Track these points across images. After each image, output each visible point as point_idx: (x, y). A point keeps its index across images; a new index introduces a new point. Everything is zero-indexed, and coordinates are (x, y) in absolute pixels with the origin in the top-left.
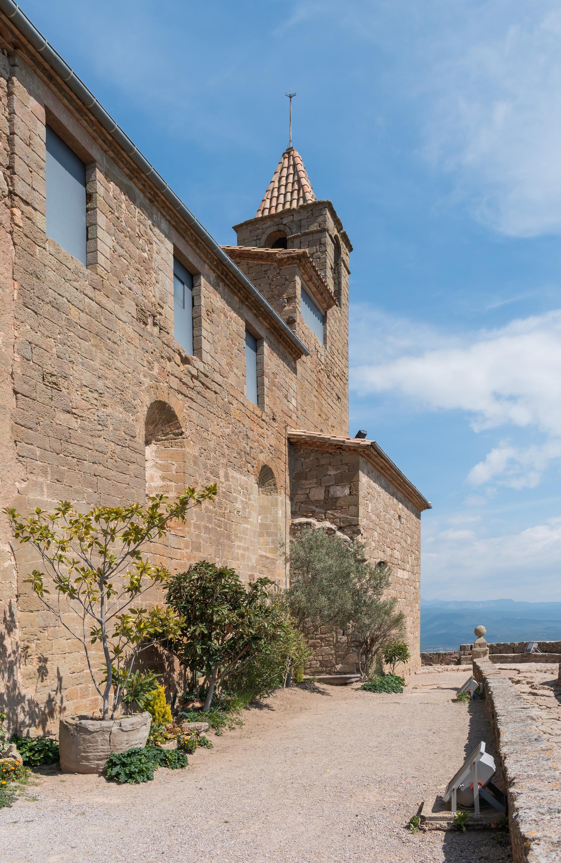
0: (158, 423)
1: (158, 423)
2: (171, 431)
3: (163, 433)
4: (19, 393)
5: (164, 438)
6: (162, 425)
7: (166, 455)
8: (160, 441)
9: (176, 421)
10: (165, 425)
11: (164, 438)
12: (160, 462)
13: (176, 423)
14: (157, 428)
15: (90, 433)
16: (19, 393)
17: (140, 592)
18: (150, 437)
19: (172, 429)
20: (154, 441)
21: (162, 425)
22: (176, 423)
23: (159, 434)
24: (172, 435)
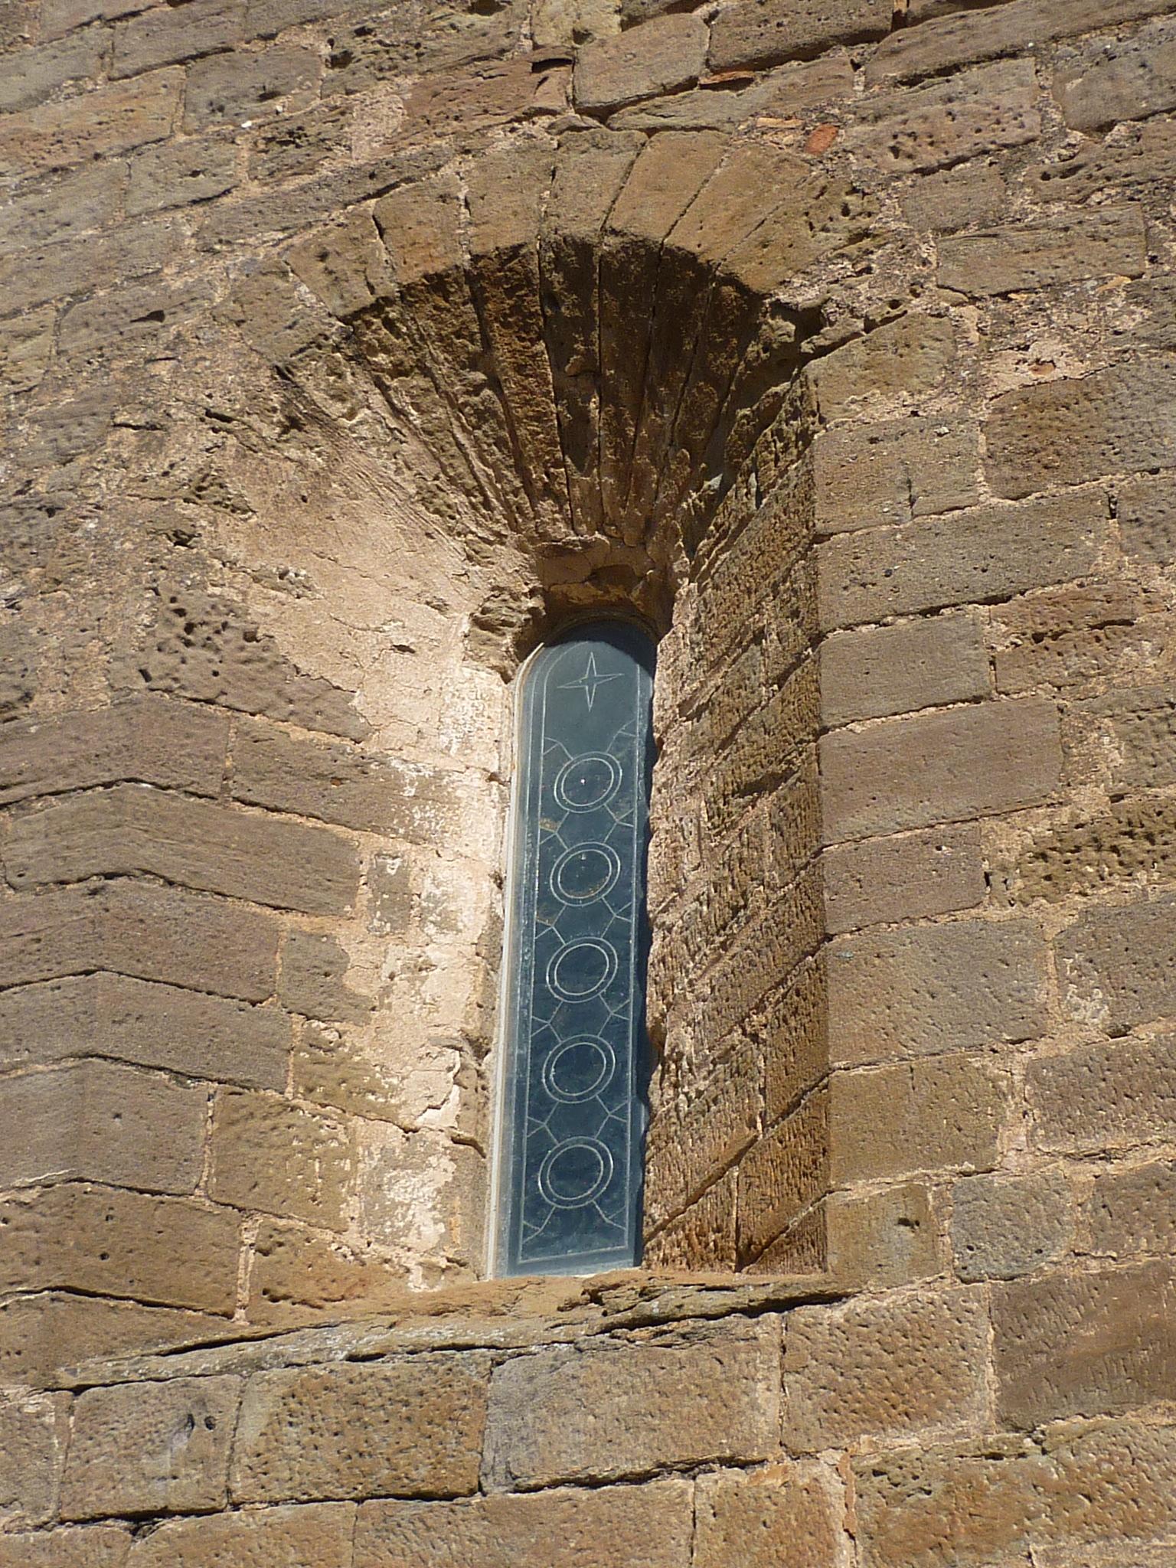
20: (681, 563)
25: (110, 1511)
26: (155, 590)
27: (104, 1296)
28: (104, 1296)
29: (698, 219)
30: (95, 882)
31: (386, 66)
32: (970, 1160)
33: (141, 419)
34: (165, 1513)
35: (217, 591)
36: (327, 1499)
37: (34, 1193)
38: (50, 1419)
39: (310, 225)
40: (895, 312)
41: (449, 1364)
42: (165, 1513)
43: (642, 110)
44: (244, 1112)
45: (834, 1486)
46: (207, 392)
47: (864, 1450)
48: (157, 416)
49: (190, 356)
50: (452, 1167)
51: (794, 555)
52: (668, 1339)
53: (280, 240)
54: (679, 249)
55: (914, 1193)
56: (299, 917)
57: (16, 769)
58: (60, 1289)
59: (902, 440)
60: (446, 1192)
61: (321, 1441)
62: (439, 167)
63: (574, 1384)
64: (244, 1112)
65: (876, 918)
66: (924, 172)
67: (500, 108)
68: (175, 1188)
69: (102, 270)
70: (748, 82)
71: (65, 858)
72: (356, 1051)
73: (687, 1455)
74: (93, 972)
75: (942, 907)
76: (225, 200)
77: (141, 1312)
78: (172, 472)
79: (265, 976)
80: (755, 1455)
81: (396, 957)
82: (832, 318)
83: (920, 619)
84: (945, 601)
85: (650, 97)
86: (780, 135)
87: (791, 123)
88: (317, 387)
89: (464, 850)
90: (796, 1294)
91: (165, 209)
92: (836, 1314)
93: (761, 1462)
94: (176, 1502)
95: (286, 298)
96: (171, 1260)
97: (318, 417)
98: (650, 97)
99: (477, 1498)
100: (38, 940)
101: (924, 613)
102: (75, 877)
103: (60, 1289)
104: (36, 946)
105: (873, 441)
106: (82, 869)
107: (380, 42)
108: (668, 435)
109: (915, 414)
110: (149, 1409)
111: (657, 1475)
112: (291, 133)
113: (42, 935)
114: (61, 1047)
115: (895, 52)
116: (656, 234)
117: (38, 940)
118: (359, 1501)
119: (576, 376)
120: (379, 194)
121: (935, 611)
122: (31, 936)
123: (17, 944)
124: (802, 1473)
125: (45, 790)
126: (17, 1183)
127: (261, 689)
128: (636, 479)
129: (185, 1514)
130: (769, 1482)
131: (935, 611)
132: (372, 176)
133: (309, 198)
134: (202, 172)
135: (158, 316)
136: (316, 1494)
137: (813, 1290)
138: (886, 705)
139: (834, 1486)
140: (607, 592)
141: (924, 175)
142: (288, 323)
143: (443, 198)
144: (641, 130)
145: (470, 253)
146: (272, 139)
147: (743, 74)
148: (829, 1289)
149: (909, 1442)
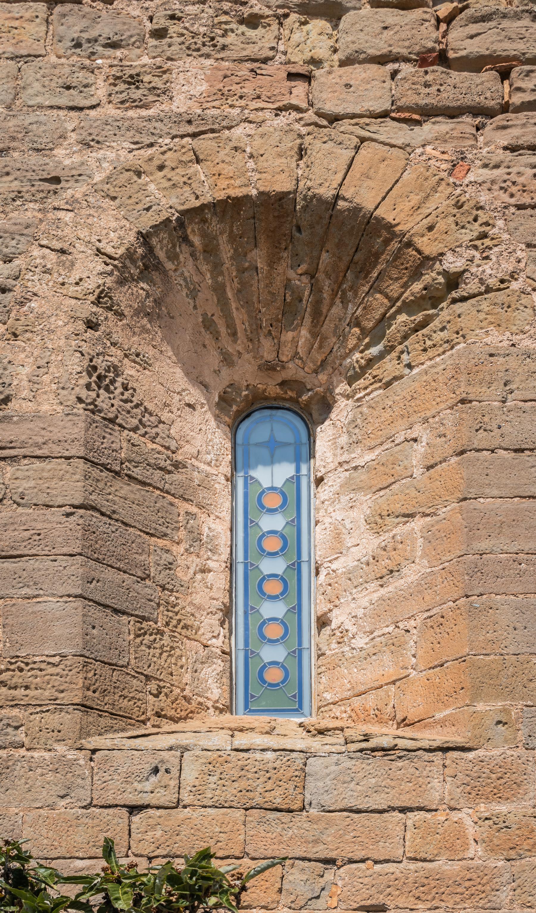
0: (318, 303)
1: (318, 303)
2: (393, 301)
3: (364, 332)
4: (448, 25)
5: (374, 351)
6: (345, 302)
7: (386, 415)
8: (364, 369)
9: (394, 245)
10: (354, 289)
11: (374, 351)
12: (369, 456)
13: (397, 255)
14: (328, 327)
15: (360, 880)
16: (448, 25)
17: (221, 610)
18: (323, 377)
19: (394, 289)
20: (342, 388)
21: (345, 302)
22: (397, 255)
23: (352, 342)
24: (402, 318)
25: (118, 803)
26: (81, 352)
27: (96, 709)
28: (96, 709)
29: (393, 202)
30: (68, 509)
31: (193, 47)
32: (531, 700)
33: (58, 245)
34: (148, 806)
35: (110, 359)
36: (231, 807)
37: (57, 659)
38: (82, 762)
39: (151, 145)
40: (502, 286)
41: (288, 758)
42: (148, 806)
43: (357, 124)
44: (142, 631)
45: (468, 822)
46: (98, 238)
47: (482, 810)
48: (66, 246)
49: (83, 212)
50: (222, 664)
51: (442, 406)
52: (393, 757)
53: (133, 150)
54: (383, 219)
55: (505, 711)
56: (156, 539)
57: (8, 439)
58: (78, 705)
59: (507, 358)
60: (221, 674)
61: (226, 783)
62: (232, 127)
63: (349, 771)
64: (142, 631)
65: (490, 591)
66: (520, 207)
67: (269, 98)
68: (121, 663)
69: (13, 139)
70: (418, 123)
71: (48, 494)
72: (184, 608)
73: (404, 805)
74: (75, 555)
75: (521, 592)
76: (93, 113)
77: (111, 718)
78: (81, 283)
79: (146, 567)
80: (434, 807)
81: (194, 562)
82: (467, 281)
83: (513, 454)
84: (527, 446)
85: (361, 116)
86: (439, 163)
87: (445, 157)
88: (161, 249)
89: (219, 515)
90: (451, 745)
91: (51, 107)
92: (471, 755)
93: (436, 810)
94: (154, 802)
95: (143, 189)
96: (121, 696)
97: (158, 267)
98: (361, 116)
99: (304, 813)
100: (39, 535)
101: (516, 451)
102: (57, 504)
103: (78, 705)
104: (38, 538)
105: (491, 355)
106: (60, 501)
107: (186, 28)
108: (348, 320)
109: (513, 345)
110: (135, 763)
111: (388, 811)
112: (131, 76)
113: (42, 532)
114: (62, 590)
115: (505, 127)
116: (369, 206)
117: (39, 535)
118: (246, 809)
119: (301, 275)
120: (194, 135)
121: (522, 450)
122: (34, 532)
123: (27, 534)
124: (455, 816)
125: (28, 454)
126: (46, 653)
127: (132, 417)
128: (321, 339)
129: (158, 808)
130: (439, 818)
131: (522, 450)
132: (189, 122)
133: (150, 126)
134: (74, 88)
135: (56, 180)
136: (226, 805)
137: (461, 745)
138: (496, 492)
139: (468, 822)
140: (286, 393)
141: (518, 209)
142: (146, 206)
143: (236, 149)
144: (357, 137)
145: (257, 189)
146: (120, 78)
147: (416, 117)
148: (467, 745)
149: (503, 808)
